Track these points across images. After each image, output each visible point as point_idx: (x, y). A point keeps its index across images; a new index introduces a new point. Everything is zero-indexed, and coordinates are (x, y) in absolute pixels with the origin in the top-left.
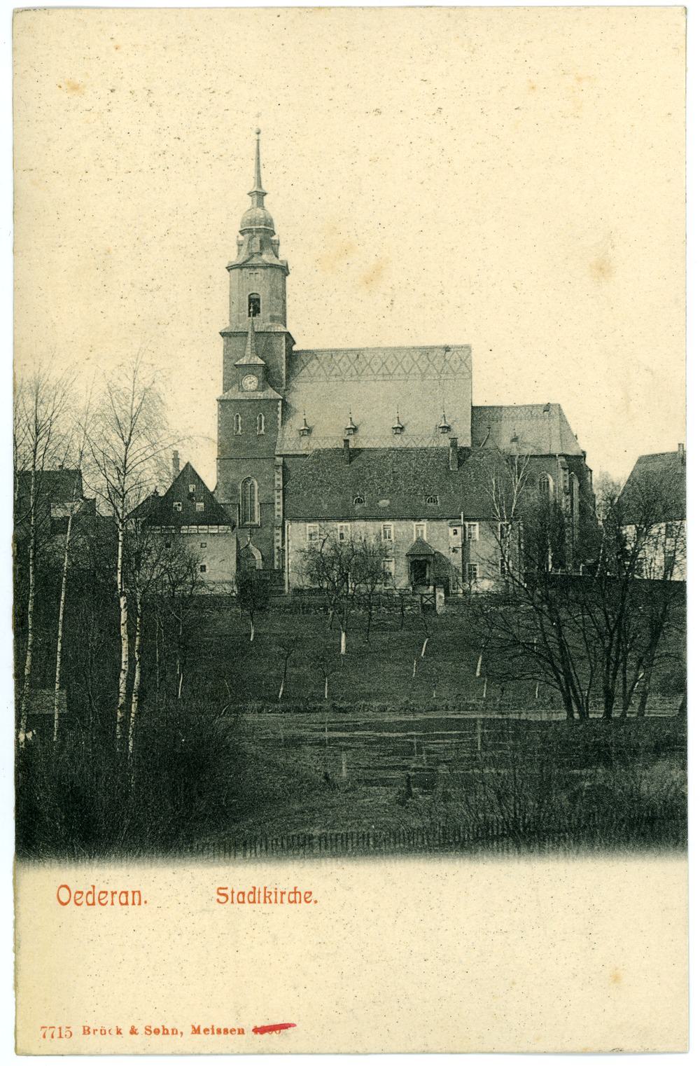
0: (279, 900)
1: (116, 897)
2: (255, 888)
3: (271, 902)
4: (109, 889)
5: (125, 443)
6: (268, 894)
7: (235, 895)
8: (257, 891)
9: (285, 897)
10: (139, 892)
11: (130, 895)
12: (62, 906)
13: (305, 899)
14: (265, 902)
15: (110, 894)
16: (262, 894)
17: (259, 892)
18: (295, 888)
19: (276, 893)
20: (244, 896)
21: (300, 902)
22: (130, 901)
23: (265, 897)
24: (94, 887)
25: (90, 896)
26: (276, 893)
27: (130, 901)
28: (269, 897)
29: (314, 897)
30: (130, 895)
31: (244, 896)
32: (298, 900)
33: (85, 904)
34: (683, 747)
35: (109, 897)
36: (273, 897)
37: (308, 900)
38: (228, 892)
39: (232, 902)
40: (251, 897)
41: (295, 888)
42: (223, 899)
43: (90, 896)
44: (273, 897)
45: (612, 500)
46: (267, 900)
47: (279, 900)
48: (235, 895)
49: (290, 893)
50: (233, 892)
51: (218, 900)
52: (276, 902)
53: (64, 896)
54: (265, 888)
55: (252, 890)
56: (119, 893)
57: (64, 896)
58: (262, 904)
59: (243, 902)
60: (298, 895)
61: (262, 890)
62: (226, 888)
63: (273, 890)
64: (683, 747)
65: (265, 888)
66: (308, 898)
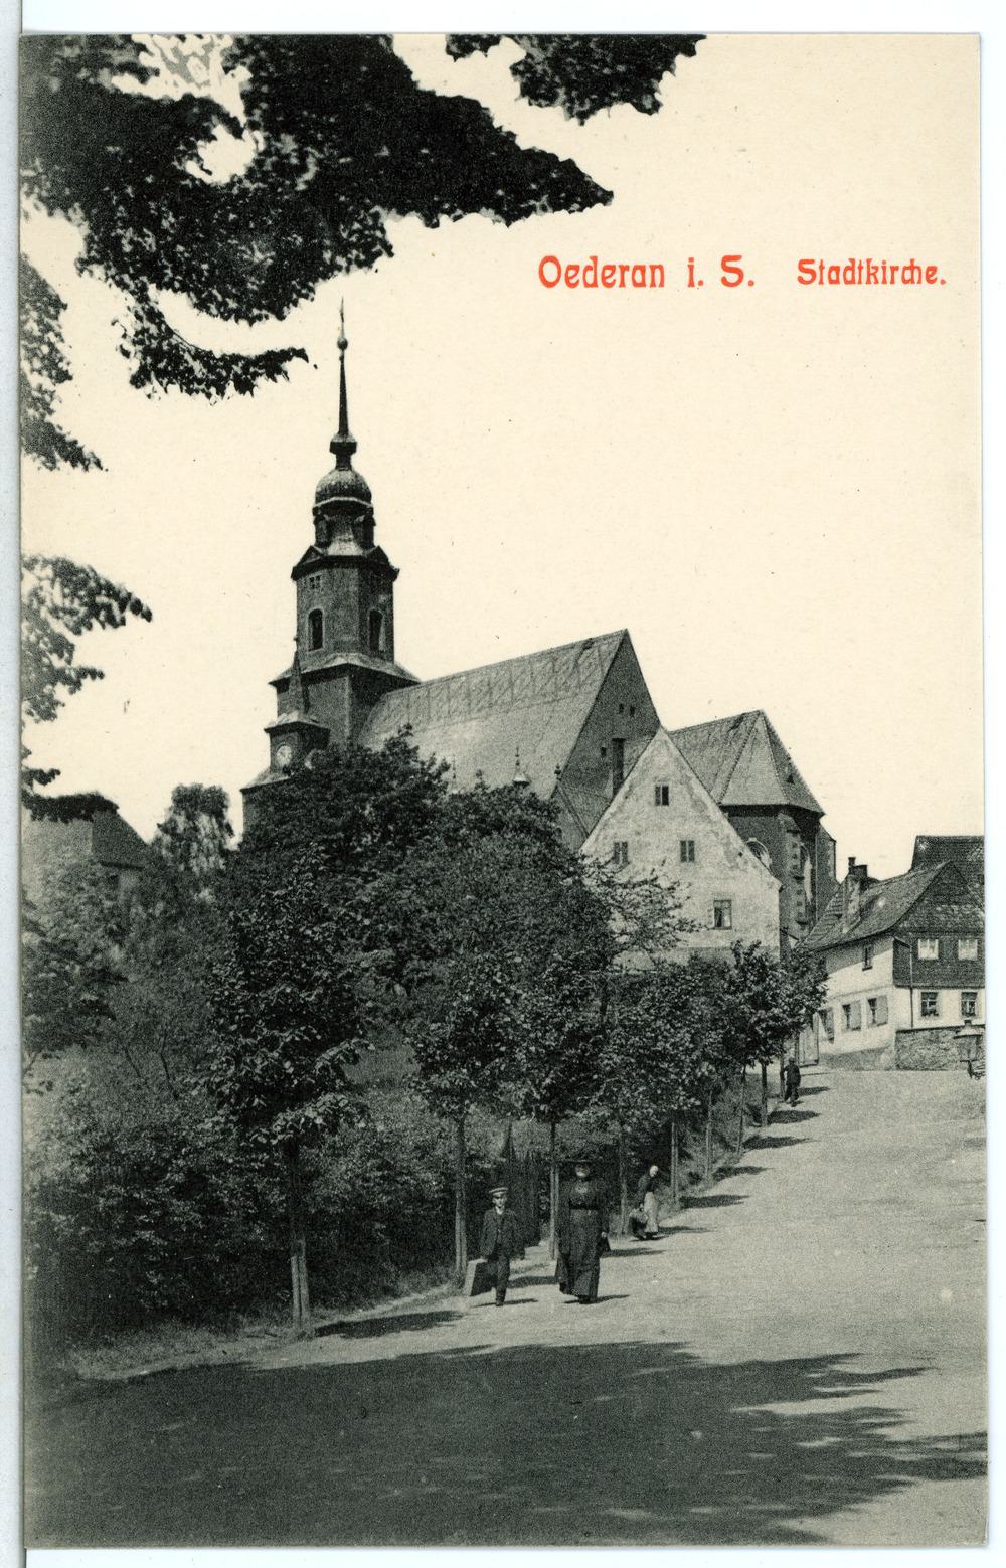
0: (889, 278)
1: (628, 275)
2: (853, 261)
3: (877, 282)
4: (616, 261)
5: (692, 1183)
6: (872, 271)
7: (826, 271)
8: (857, 264)
9: (898, 275)
10: (661, 267)
11: (648, 271)
12: (543, 287)
13: (604, 278)
14: (869, 282)
15: (618, 270)
16: (864, 271)
17: (861, 267)
18: (912, 261)
19: (884, 268)
20: (837, 273)
21: (920, 282)
22: (648, 281)
23: (869, 274)
24: (594, 259)
25: (590, 274)
26: (884, 268)
27: (648, 281)
28: (874, 274)
29: (939, 275)
30: (648, 271)
31: (837, 273)
32: (916, 278)
33: (581, 283)
34: (978, 1456)
35: (617, 275)
36: (880, 275)
37: (609, 280)
38: (815, 267)
39: (821, 282)
40: (849, 275)
41: (912, 261)
42: (807, 277)
43: (590, 274)
44: (880, 275)
45: (461, 1094)
46: (872, 278)
47: (889, 278)
48: (826, 271)
49: (905, 268)
50: (822, 267)
51: (724, 281)
52: (885, 281)
53: (551, 271)
54: (869, 261)
55: (850, 264)
56: (724, 273)
57: (551, 271)
58: (864, 284)
59: (594, 284)
60: (916, 271)
61: (865, 265)
62: (812, 262)
63: (880, 264)
64: (978, 1456)
65: (869, 261)
66: (572, 277)
